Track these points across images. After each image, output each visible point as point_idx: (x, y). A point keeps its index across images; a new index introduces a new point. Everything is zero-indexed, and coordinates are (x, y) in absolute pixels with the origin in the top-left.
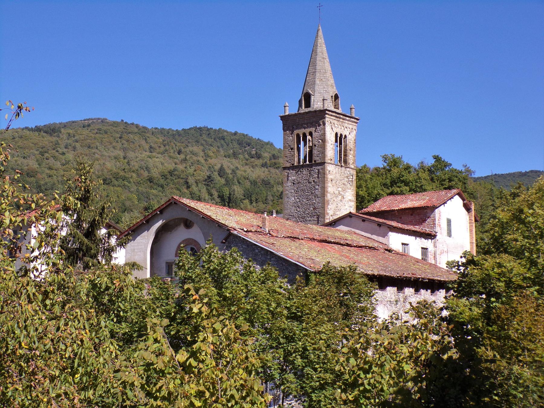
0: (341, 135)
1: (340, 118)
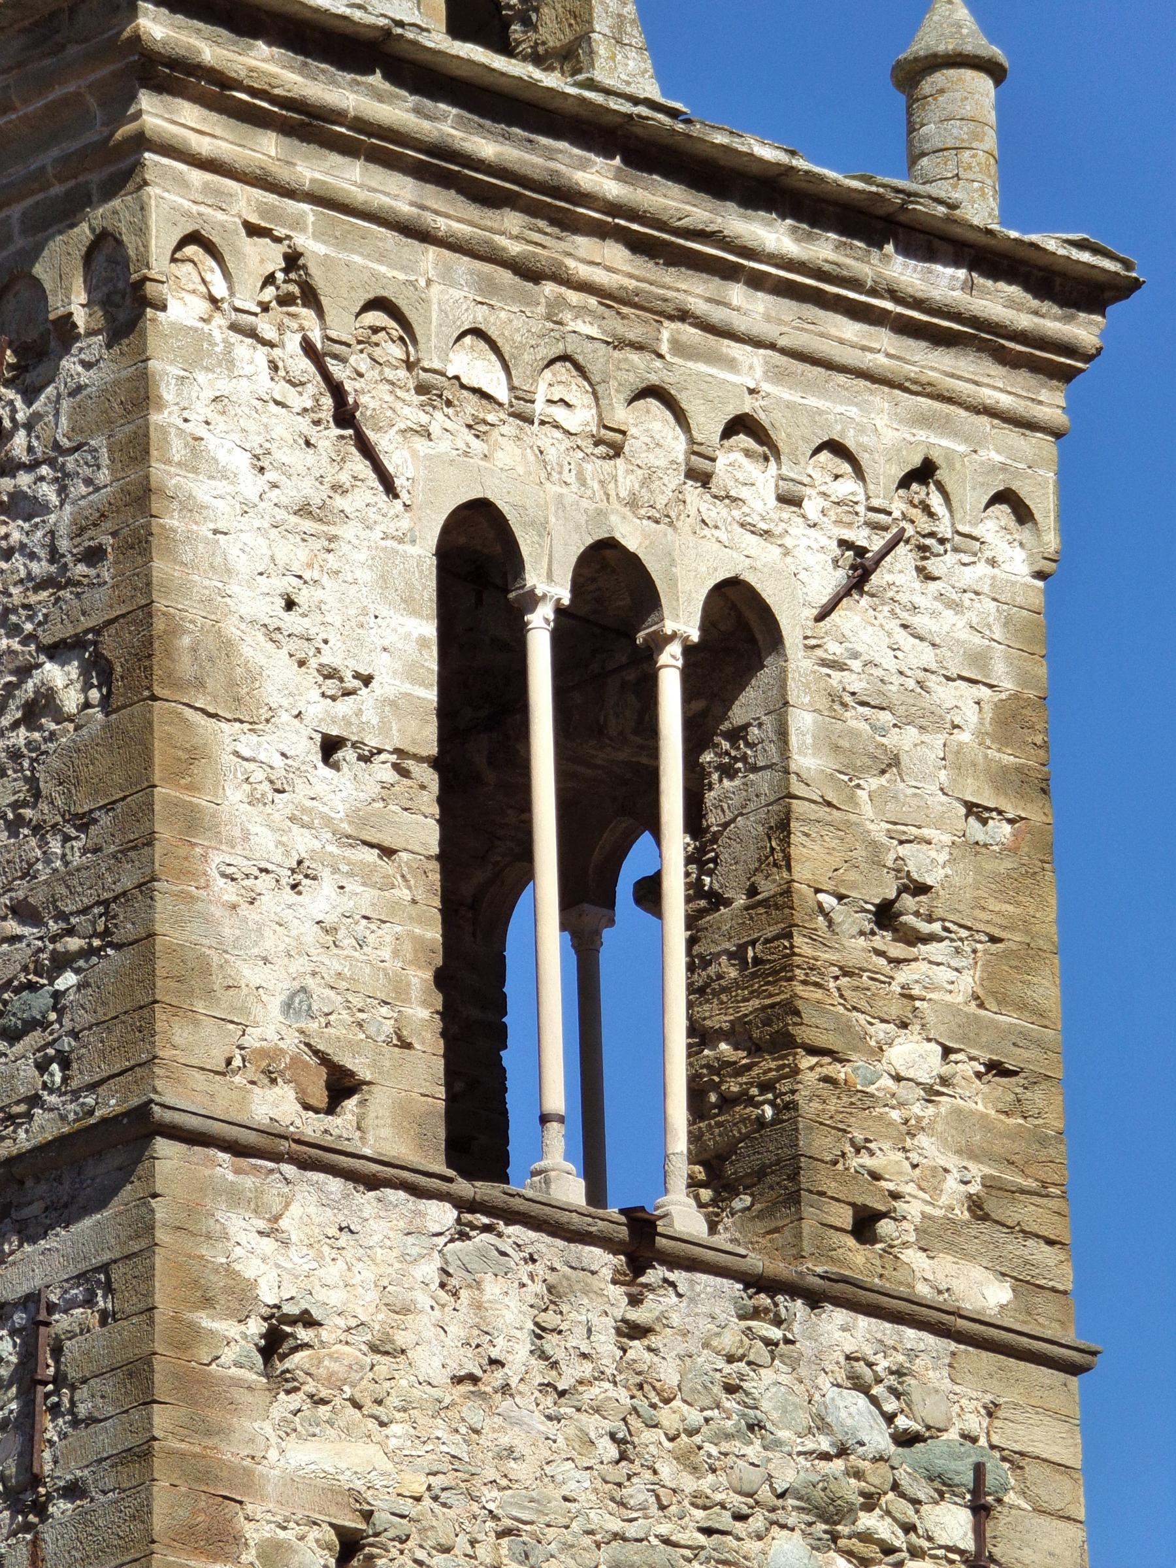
0: (614, 584)
1: (559, 207)
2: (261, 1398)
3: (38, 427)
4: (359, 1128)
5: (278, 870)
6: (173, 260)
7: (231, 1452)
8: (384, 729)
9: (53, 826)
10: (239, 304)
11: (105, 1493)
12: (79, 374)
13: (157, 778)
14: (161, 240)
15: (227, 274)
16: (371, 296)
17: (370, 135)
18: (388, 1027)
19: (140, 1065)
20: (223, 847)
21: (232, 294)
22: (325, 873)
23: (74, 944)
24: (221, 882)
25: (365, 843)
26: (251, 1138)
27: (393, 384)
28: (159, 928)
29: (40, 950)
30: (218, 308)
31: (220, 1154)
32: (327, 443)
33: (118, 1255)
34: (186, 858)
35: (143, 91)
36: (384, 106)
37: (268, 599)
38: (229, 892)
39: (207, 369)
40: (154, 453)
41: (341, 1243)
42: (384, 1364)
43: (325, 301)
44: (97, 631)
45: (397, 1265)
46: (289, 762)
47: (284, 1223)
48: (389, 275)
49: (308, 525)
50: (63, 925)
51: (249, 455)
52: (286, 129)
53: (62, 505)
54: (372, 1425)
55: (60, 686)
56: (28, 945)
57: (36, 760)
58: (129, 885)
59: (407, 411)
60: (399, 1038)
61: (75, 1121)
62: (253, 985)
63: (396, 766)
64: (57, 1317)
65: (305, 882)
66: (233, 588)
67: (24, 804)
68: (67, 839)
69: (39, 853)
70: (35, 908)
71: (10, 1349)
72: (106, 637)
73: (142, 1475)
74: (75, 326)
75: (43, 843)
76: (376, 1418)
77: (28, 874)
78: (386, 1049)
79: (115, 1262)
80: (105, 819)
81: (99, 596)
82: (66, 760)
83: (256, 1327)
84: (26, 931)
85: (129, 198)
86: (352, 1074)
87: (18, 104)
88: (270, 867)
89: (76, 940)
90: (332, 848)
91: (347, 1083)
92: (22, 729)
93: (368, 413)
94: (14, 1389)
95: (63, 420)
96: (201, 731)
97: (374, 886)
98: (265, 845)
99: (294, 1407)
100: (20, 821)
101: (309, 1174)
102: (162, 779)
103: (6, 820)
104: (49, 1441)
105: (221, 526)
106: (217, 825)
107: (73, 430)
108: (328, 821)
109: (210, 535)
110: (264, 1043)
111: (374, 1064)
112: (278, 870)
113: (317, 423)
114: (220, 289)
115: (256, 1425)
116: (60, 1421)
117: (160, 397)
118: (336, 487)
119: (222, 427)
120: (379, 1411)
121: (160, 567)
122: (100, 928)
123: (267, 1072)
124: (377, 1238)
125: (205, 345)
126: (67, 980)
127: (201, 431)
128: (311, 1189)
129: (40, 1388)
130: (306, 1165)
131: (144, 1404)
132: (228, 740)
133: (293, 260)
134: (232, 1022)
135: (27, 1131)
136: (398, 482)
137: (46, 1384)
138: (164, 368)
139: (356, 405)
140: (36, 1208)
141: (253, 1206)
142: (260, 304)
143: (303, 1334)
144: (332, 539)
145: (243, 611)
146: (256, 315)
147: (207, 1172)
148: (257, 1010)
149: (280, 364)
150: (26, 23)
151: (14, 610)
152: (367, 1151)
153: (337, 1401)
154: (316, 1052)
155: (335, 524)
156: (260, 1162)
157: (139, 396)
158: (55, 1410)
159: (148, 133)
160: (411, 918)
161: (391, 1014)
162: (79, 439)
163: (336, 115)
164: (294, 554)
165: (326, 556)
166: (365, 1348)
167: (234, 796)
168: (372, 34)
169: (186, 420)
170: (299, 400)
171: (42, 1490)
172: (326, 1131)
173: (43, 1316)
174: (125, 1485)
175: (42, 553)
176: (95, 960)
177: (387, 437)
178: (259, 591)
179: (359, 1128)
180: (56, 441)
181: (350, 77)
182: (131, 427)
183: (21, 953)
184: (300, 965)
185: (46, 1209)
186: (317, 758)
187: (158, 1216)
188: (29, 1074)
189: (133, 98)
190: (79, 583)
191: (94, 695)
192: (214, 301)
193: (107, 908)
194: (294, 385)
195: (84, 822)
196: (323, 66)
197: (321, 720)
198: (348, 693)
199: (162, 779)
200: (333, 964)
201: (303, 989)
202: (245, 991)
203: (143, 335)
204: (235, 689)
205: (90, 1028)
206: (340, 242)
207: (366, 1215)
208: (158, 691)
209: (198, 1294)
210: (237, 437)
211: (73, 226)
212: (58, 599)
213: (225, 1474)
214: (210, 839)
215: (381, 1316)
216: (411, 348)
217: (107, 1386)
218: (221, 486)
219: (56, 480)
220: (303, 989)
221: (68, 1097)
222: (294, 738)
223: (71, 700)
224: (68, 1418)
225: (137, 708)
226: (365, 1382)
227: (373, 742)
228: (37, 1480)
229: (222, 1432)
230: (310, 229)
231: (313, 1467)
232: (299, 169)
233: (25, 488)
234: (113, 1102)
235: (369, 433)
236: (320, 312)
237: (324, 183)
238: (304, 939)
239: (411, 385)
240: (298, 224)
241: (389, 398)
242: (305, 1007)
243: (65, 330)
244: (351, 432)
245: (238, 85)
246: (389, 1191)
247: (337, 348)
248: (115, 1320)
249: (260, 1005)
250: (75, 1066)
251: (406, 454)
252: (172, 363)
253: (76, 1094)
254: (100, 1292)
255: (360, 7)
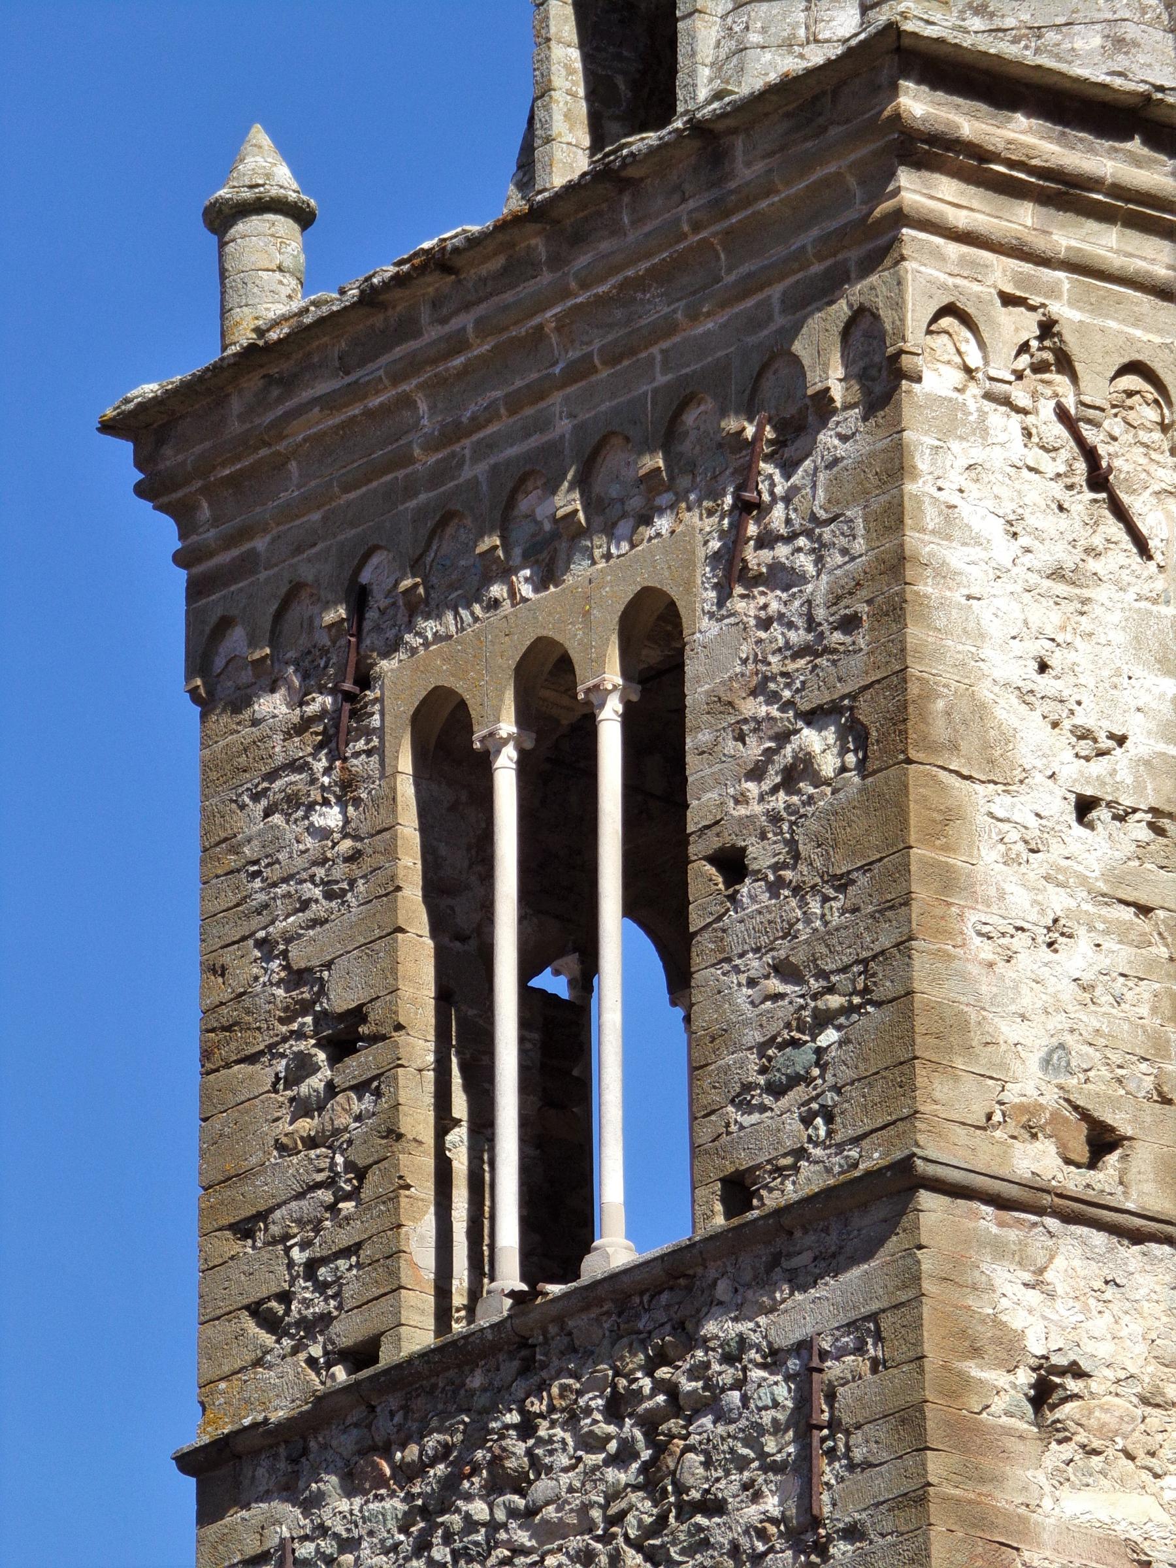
2: (1034, 1447)
3: (796, 500)
4: (1121, 1183)
5: (1034, 928)
6: (929, 332)
7: (1006, 1499)
8: (1139, 787)
9: (813, 887)
10: (993, 373)
11: (883, 1536)
12: (835, 447)
13: (913, 839)
14: (917, 313)
15: (982, 344)
16: (1126, 360)
17: (1128, 201)
18: (1148, 1083)
19: (902, 1119)
20: (979, 907)
21: (986, 362)
22: (1081, 931)
23: (834, 1001)
24: (978, 940)
25: (1121, 901)
26: (1014, 1192)
27: (1147, 446)
28: (917, 986)
29: (802, 1008)
30: (973, 378)
31: (983, 1207)
32: (1081, 507)
33: (886, 1305)
34: (942, 918)
35: (901, 168)
36: (1142, 172)
37: (1022, 662)
38: (985, 950)
39: (961, 438)
40: (908, 522)
41: (1108, 1296)
42: (1156, 1418)
43: (1079, 367)
44: (853, 696)
45: (1165, 1319)
46: (1044, 822)
47: (1049, 1276)
48: (1145, 339)
49: (1061, 589)
50: (823, 983)
51: (1002, 521)
52: (1044, 199)
53: (818, 575)
54: (1146, 1477)
55: (818, 751)
56: (791, 1003)
57: (795, 823)
58: (888, 944)
59: (1161, 473)
60: (1160, 1094)
61: (840, 1173)
62: (1011, 1041)
63: (1151, 825)
64: (829, 1363)
65: (1061, 940)
66: (986, 652)
67: (784, 866)
68: (826, 899)
69: (799, 913)
70: (796, 967)
71: (786, 1394)
72: (861, 703)
73: (919, 1519)
74: (832, 400)
75: (803, 904)
76: (1150, 1470)
77: (789, 934)
78: (1147, 1105)
79: (884, 1311)
80: (863, 880)
81: (855, 663)
82: (824, 822)
83: (1025, 1377)
84: (788, 989)
85: (886, 273)
86: (1112, 1129)
87: (780, 187)
88: (1026, 926)
89: (836, 997)
90: (1087, 907)
91: (1109, 1138)
92: (782, 794)
93: (1122, 476)
94: (791, 1433)
95: (821, 493)
96: (956, 793)
97: (1130, 943)
98: (1020, 904)
99: (1067, 1456)
100: (780, 883)
101: (1073, 1228)
102: (917, 840)
103: (767, 882)
104: (827, 1484)
105: (974, 591)
106: (973, 885)
107: (829, 501)
108: (1083, 881)
109: (963, 600)
110: (1023, 1099)
111: (1135, 1120)
112: (1034, 928)
113: (1070, 487)
114: (974, 358)
115: (1029, 1474)
116: (837, 1465)
117: (914, 467)
118: (1089, 551)
119: (975, 494)
120: (1152, 1462)
121: (914, 633)
122: (860, 986)
123: (1028, 1127)
124: (1143, 1291)
125: (960, 415)
126: (829, 1037)
127: (955, 499)
128: (1075, 1242)
129: (815, 1432)
130: (1068, 1218)
131: (917, 1450)
132: (982, 802)
133: (1047, 328)
134: (991, 1078)
135: (794, 1183)
136: (1152, 544)
137: (821, 1428)
138: (919, 439)
139: (1110, 469)
140: (805, 1258)
141: (1017, 1258)
142: (1014, 372)
143: (1073, 1385)
144: (1085, 601)
145: (997, 674)
146: (1010, 383)
147: (971, 1225)
148: (1016, 1066)
149: (1034, 431)
150: (790, 108)
151: (773, 678)
152: (1130, 1206)
153: (1110, 1452)
154: (1076, 1108)
155: (1087, 586)
156: (1023, 1215)
157: (894, 466)
158: (831, 1454)
159: (906, 210)
160: (1169, 975)
161: (1151, 1070)
162: (837, 510)
163: (1094, 183)
164: (1048, 617)
165: (1079, 618)
166: (1135, 1400)
167: (989, 856)
168: (1132, 101)
169: (940, 489)
170: (1052, 466)
171: (822, 1532)
172: (1088, 1186)
173: (815, 1362)
174: (903, 1529)
175: (800, 622)
176: (855, 1017)
177: (1141, 499)
178: (1012, 655)
179: (1121, 1183)
180: (813, 514)
181: (1108, 144)
182: (886, 497)
183: (784, 1010)
184: (1058, 1021)
185: (815, 1259)
186: (1072, 817)
187: (924, 1267)
188: (794, 1127)
189: (892, 175)
190: (835, 651)
191: (851, 759)
192: (968, 370)
193: (866, 966)
194: (1048, 451)
195: (842, 883)
196: (1081, 135)
197: (1075, 780)
198: (1102, 754)
199: (917, 840)
200: (1090, 1021)
201: (1061, 1046)
202: (1003, 1047)
203: (898, 407)
204: (989, 751)
205: (852, 1083)
206: (1096, 308)
207: (1131, 1269)
208: (913, 754)
209: (967, 1344)
210: (990, 504)
211: (831, 303)
212: (815, 667)
213: (1000, 1521)
214: (966, 899)
215: (1150, 1369)
216: (1166, 411)
217: (880, 1431)
218: (975, 553)
219: (813, 550)
220: (1061, 1046)
221: (833, 1150)
222: (1047, 798)
223: (828, 765)
224: (844, 1462)
225: (892, 771)
226: (1137, 1434)
227: (1127, 801)
228: (816, 1522)
229: (997, 1480)
230: (1065, 297)
231: (1088, 1516)
232: (1055, 237)
233: (783, 560)
234: (876, 1155)
235: (1125, 498)
236: (1074, 378)
237: (1080, 250)
238: (1061, 997)
239: (1166, 446)
240: (1053, 291)
241: (1143, 460)
242: (1063, 1064)
243: (823, 404)
244: (1104, 495)
245: (996, 157)
246: (1153, 1245)
247: (1091, 413)
248: (886, 1368)
249: (1019, 1061)
250: (838, 1120)
251: (1160, 515)
252: (926, 433)
253: (840, 1147)
254: (870, 1341)
255: (1120, 74)
